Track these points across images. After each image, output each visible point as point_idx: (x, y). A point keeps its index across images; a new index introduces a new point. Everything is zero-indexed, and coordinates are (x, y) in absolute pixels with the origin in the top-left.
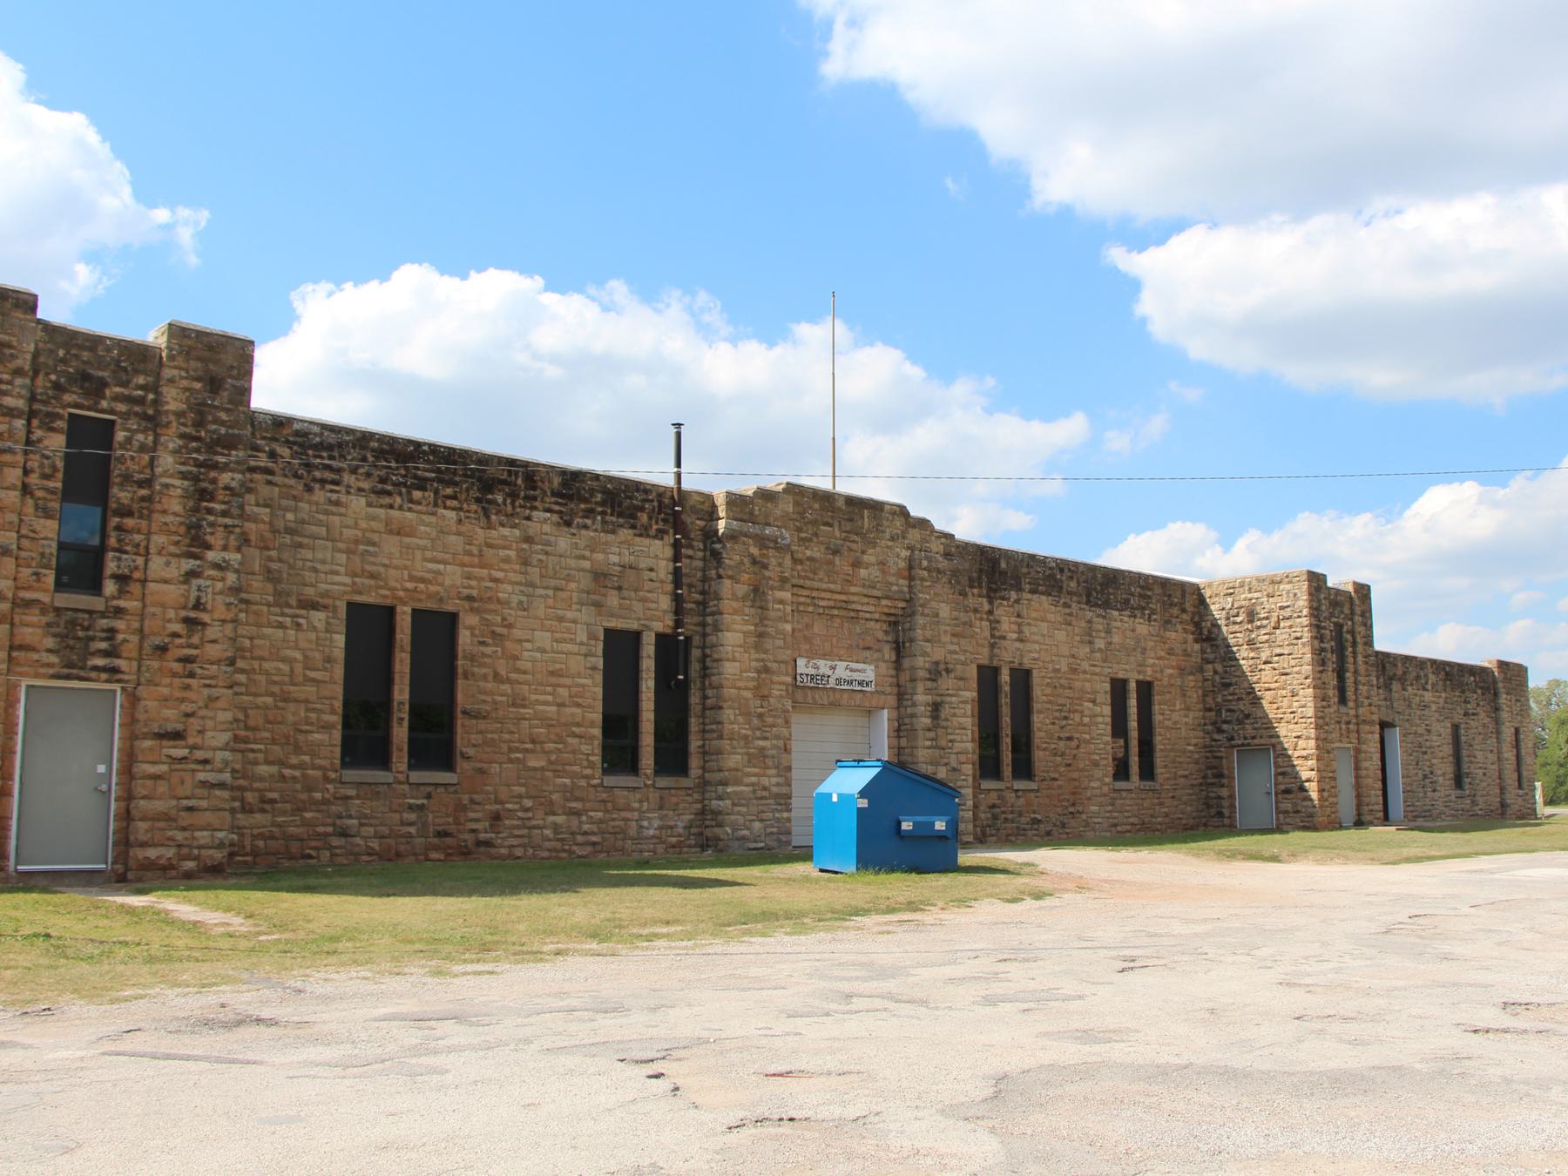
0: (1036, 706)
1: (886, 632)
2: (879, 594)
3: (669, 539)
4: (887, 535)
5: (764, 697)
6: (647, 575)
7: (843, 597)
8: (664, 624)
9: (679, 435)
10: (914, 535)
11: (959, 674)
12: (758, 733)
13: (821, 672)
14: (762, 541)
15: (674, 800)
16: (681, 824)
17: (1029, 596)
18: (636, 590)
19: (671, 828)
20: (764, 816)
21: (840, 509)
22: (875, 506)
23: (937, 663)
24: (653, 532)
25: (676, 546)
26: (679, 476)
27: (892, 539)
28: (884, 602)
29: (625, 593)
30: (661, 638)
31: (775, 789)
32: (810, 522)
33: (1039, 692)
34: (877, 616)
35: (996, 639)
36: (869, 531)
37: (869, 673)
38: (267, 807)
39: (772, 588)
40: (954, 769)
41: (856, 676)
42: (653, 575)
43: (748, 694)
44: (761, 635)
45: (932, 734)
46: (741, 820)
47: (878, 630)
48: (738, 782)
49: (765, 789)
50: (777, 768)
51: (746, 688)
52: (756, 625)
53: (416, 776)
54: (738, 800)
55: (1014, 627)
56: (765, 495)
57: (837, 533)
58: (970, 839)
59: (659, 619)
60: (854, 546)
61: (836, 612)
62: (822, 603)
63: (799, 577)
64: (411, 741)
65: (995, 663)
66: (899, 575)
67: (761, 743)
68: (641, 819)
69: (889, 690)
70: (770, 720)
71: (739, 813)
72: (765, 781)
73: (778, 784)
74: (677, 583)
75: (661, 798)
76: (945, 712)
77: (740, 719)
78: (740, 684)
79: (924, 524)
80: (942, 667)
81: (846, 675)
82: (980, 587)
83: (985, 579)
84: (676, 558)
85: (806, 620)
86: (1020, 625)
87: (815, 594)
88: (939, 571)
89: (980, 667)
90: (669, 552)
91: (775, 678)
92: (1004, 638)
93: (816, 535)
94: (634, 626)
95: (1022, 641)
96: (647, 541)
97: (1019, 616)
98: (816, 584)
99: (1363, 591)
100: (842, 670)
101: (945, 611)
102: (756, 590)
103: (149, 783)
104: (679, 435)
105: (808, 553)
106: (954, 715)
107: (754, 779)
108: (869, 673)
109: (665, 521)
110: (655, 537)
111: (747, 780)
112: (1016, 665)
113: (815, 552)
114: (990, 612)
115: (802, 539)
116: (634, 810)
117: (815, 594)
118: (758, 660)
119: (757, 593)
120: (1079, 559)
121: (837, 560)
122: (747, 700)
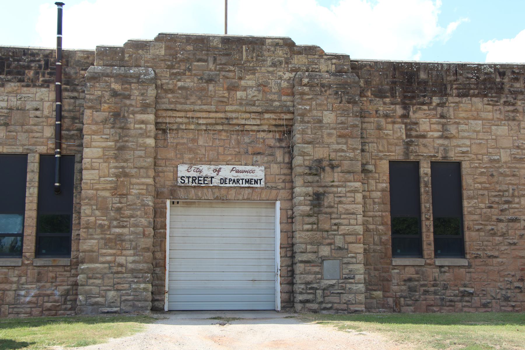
0: (465, 193)
1: (280, 140)
2: (259, 109)
3: (52, 86)
4: (269, 63)
5: (122, 195)
6: (32, 113)
8: (47, 147)
9: (60, 12)
10: (299, 61)
12: (115, 223)
13: (204, 174)
14: (124, 79)
15: (51, 275)
16: (57, 293)
17: (457, 99)
18: (22, 125)
19: (48, 296)
20: (120, 287)
21: (216, 48)
23: (320, 161)
24: (40, 82)
25: (59, 91)
26: (59, 40)
27: (274, 65)
28: (267, 116)
29: (12, 128)
30: (44, 159)
31: (130, 266)
32: (182, 61)
33: (469, 181)
34: (266, 128)
35: (412, 137)
39: (134, 113)
40: (340, 248)
42: (38, 113)
43: (107, 194)
44: (121, 149)
45: (313, 219)
46: (95, 290)
47: (271, 139)
48: (92, 261)
51: (105, 189)
52: (117, 141)
53: (439, 262)
54: (91, 275)
56: (137, 45)
57: (211, 66)
58: (362, 308)
59: (42, 144)
60: (231, 74)
61: (220, 127)
62: (201, 121)
63: (170, 103)
64: (435, 240)
65: (412, 158)
66: (281, 92)
67: (118, 230)
68: (19, 289)
69: (281, 185)
70: (128, 213)
71: (93, 284)
72: (121, 260)
73: (134, 262)
74: (60, 117)
75: (39, 273)
77: (97, 213)
78: (97, 186)
79: (311, 51)
80: (325, 163)
81: (233, 175)
82: (393, 96)
83: (399, 89)
84: (59, 98)
85: (191, 136)
86: (443, 125)
87: (190, 115)
90: (53, 96)
91: (134, 180)
92: (424, 137)
93: (190, 70)
94: (20, 150)
95: (447, 138)
96: (34, 90)
97: (442, 117)
98: (187, 107)
102: (117, 115)
103: (302, 265)
104: (60, 12)
105: (180, 84)
106: (340, 202)
107: (109, 258)
108: (259, 173)
109: (50, 74)
110: (42, 86)
111: (102, 259)
112: (439, 157)
113: (188, 82)
116: (12, 283)
117: (190, 115)
118: (116, 168)
119: (118, 117)
120: (440, 61)
121: (211, 87)
122: (105, 198)
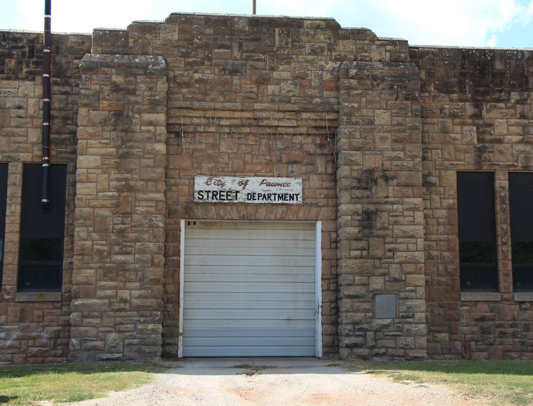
2: (296, 107)
4: (308, 50)
5: (125, 214)
6: (14, 113)
7: (249, 115)
10: (345, 47)
11: (402, 180)
12: (117, 248)
13: (227, 188)
14: (128, 70)
16: (45, 335)
19: (34, 338)
20: (122, 327)
22: (291, 26)
23: (371, 171)
24: (23, 74)
25: (47, 85)
26: (48, 22)
27: (314, 52)
28: (305, 116)
30: (29, 169)
31: (135, 302)
32: (200, 47)
34: (303, 130)
36: (281, 47)
37: (295, 186)
38: (368, 320)
39: (140, 112)
40: (396, 280)
41: (273, 190)
42: (21, 112)
43: (106, 212)
44: (124, 156)
46: (92, 331)
47: (310, 144)
48: (88, 296)
49: (124, 301)
50: (141, 280)
52: (118, 147)
53: (518, 296)
54: (87, 313)
55: (519, 130)
56: (142, 28)
57: (236, 54)
59: (26, 151)
60: (261, 64)
61: (247, 130)
62: (223, 122)
65: (485, 168)
67: (120, 257)
69: (323, 202)
70: (132, 235)
71: (89, 325)
72: (124, 294)
73: (140, 297)
74: (48, 117)
75: (22, 311)
76: (382, 219)
77: (95, 236)
80: (377, 174)
81: (263, 189)
82: (462, 91)
84: (47, 93)
85: (211, 140)
86: (524, 127)
87: (209, 114)
88: (374, 78)
89: (460, 175)
90: (39, 90)
91: (140, 196)
92: (500, 141)
93: (209, 59)
96: (16, 83)
98: (206, 105)
99: (94, 30)
100: (255, 184)
101: (382, 117)
105: (197, 76)
106: (396, 223)
107: (109, 292)
108: (295, 186)
109: (36, 64)
110: (26, 79)
111: (100, 293)
113: (208, 74)
114: (477, 116)
115: (189, 64)
117: (209, 114)
118: (118, 180)
120: (511, 48)
121: (236, 80)
122: (104, 218)
